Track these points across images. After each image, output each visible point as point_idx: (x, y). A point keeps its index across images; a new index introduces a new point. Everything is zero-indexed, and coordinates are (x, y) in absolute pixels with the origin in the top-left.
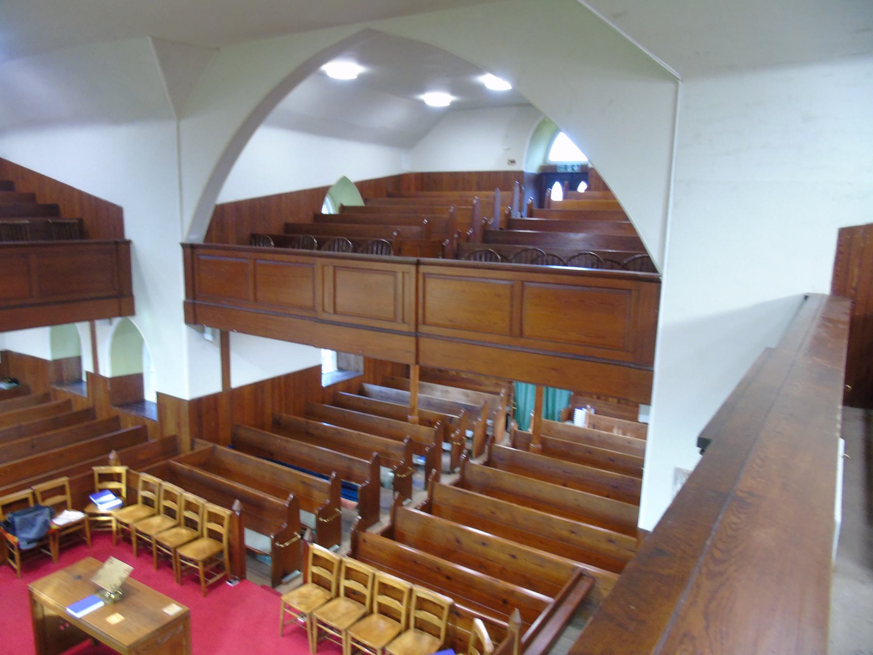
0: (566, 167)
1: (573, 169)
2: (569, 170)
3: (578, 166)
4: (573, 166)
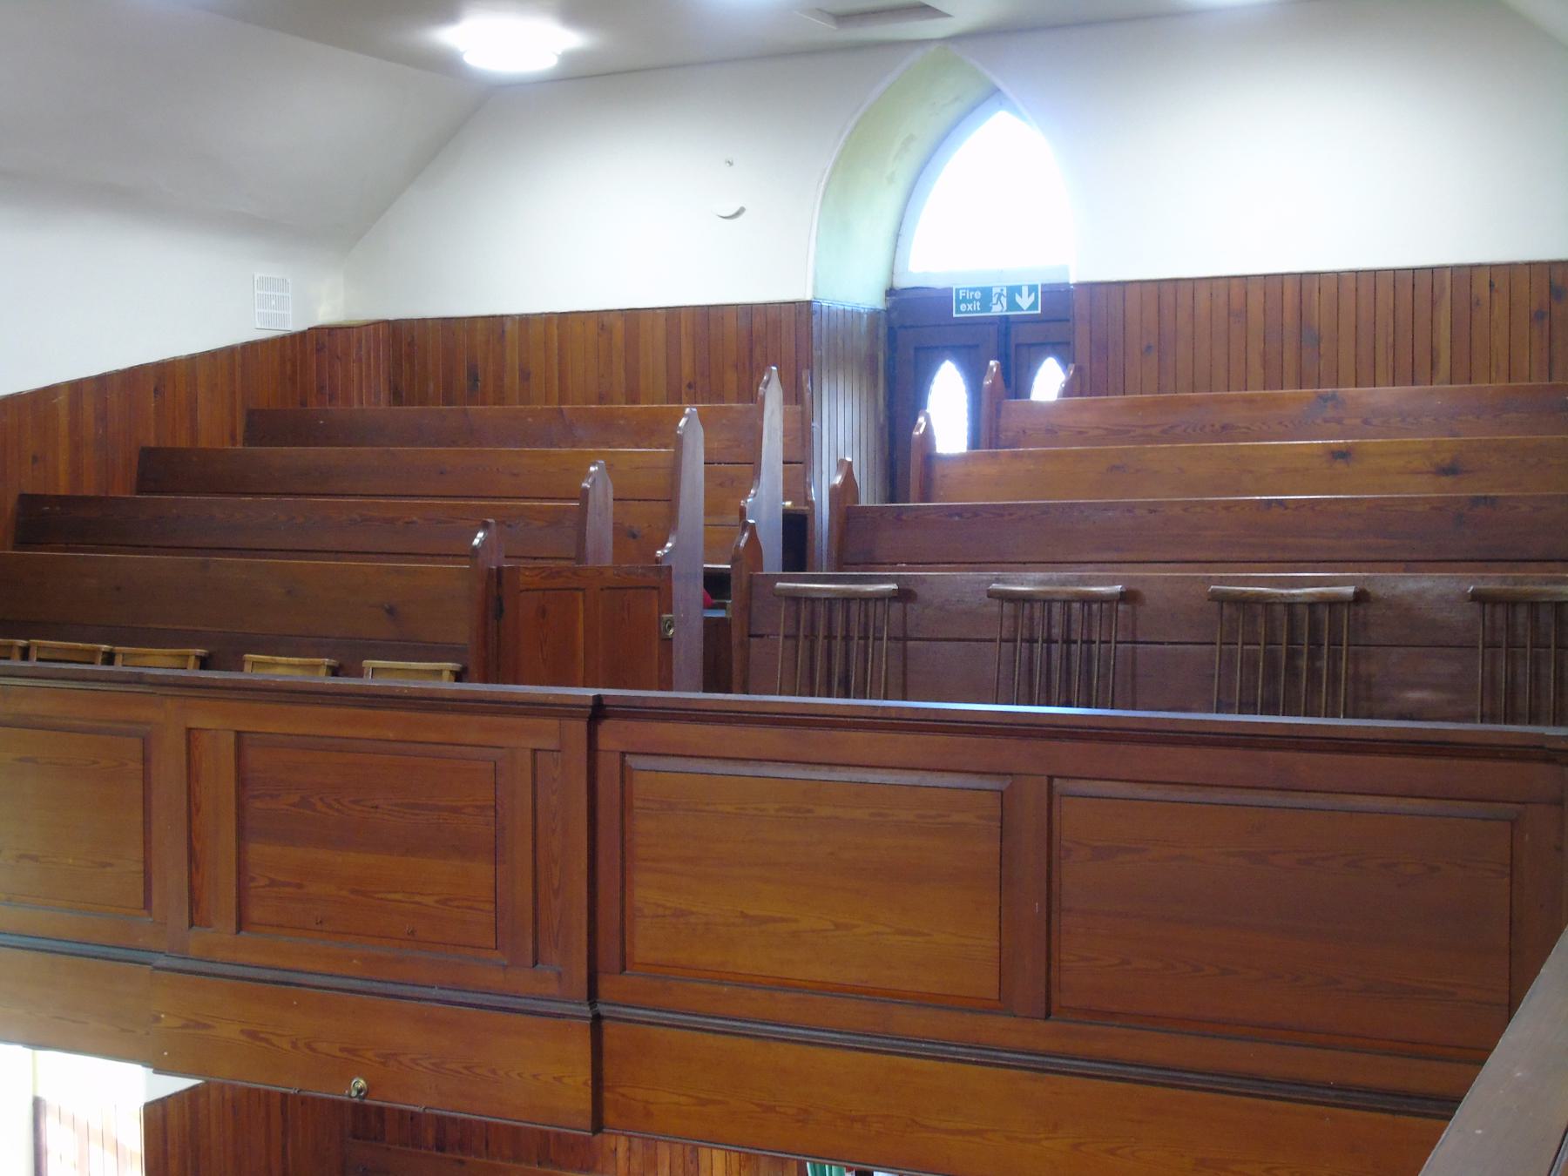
0: (986, 294)
1: (1012, 304)
2: (998, 309)
3: (1032, 289)
4: (1014, 291)
